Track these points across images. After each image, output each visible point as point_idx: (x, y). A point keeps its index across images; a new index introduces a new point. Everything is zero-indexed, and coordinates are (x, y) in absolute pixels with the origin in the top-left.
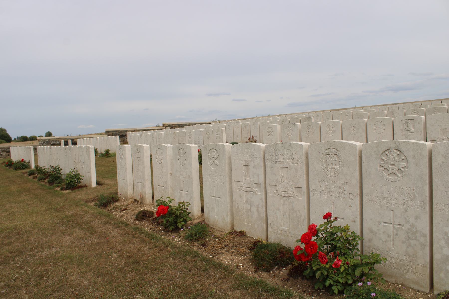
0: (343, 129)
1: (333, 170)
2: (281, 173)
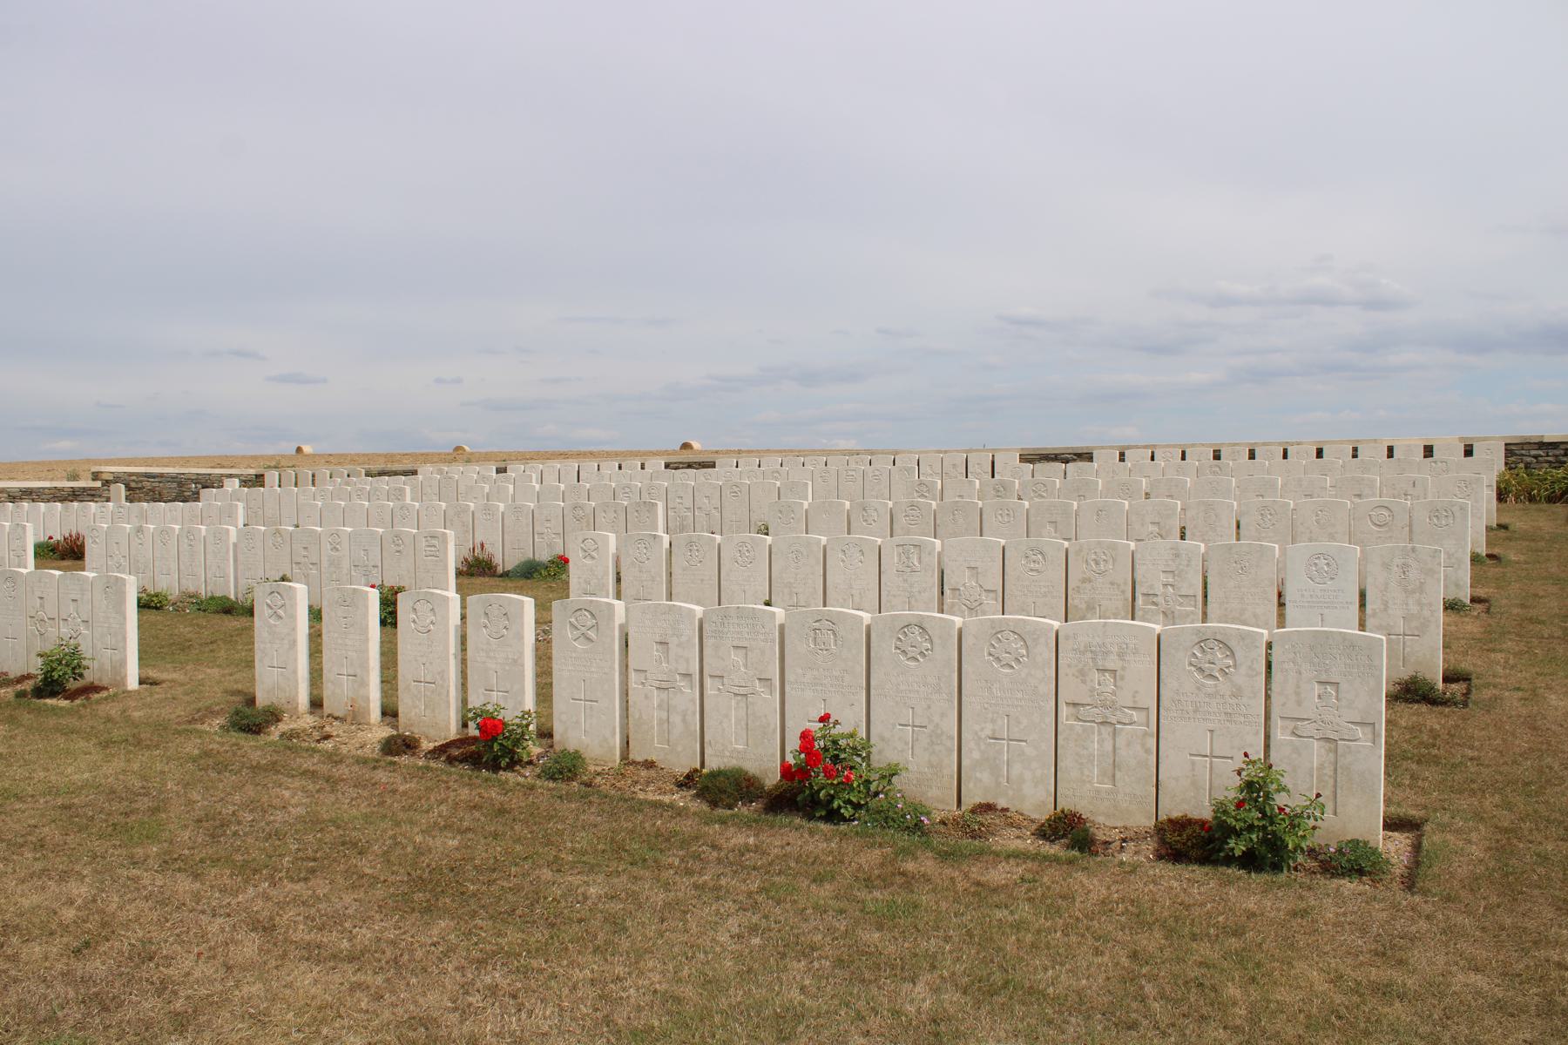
0: (773, 556)
1: (825, 652)
2: (732, 657)
